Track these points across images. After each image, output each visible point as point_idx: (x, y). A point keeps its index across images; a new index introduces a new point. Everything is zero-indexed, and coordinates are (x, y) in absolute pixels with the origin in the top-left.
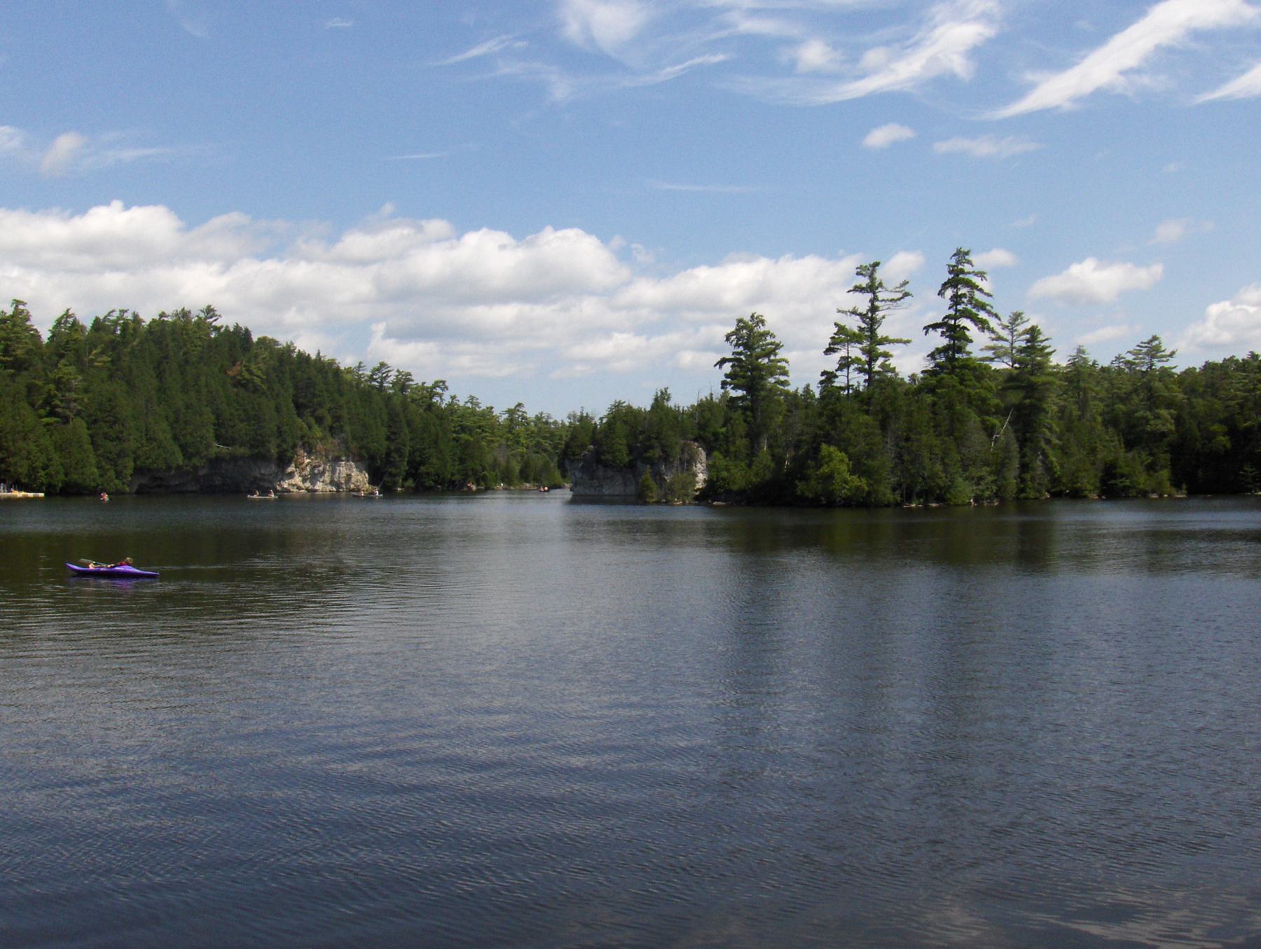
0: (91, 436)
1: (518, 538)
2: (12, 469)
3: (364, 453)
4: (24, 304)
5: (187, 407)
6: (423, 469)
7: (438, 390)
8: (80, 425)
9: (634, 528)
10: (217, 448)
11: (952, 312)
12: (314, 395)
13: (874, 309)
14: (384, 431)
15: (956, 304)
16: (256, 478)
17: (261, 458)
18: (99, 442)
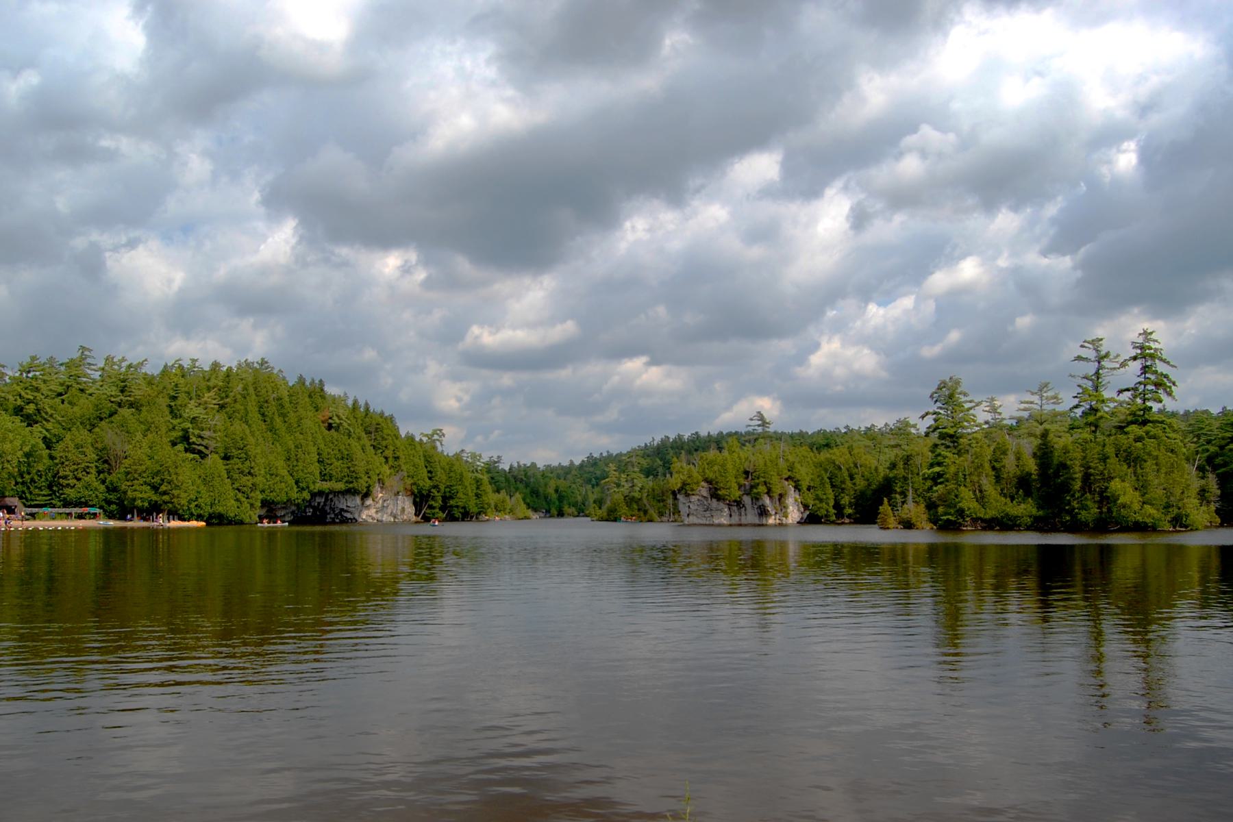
0: (228, 472)
1: (531, 554)
2: (175, 500)
3: (414, 488)
4: (90, 350)
5: (296, 447)
6: (452, 502)
7: (436, 437)
8: (214, 460)
9: (664, 558)
10: (320, 485)
11: (1141, 379)
12: (383, 439)
13: (1097, 374)
14: (425, 474)
15: (1145, 373)
16: (342, 510)
17: (352, 492)
18: (236, 476)
